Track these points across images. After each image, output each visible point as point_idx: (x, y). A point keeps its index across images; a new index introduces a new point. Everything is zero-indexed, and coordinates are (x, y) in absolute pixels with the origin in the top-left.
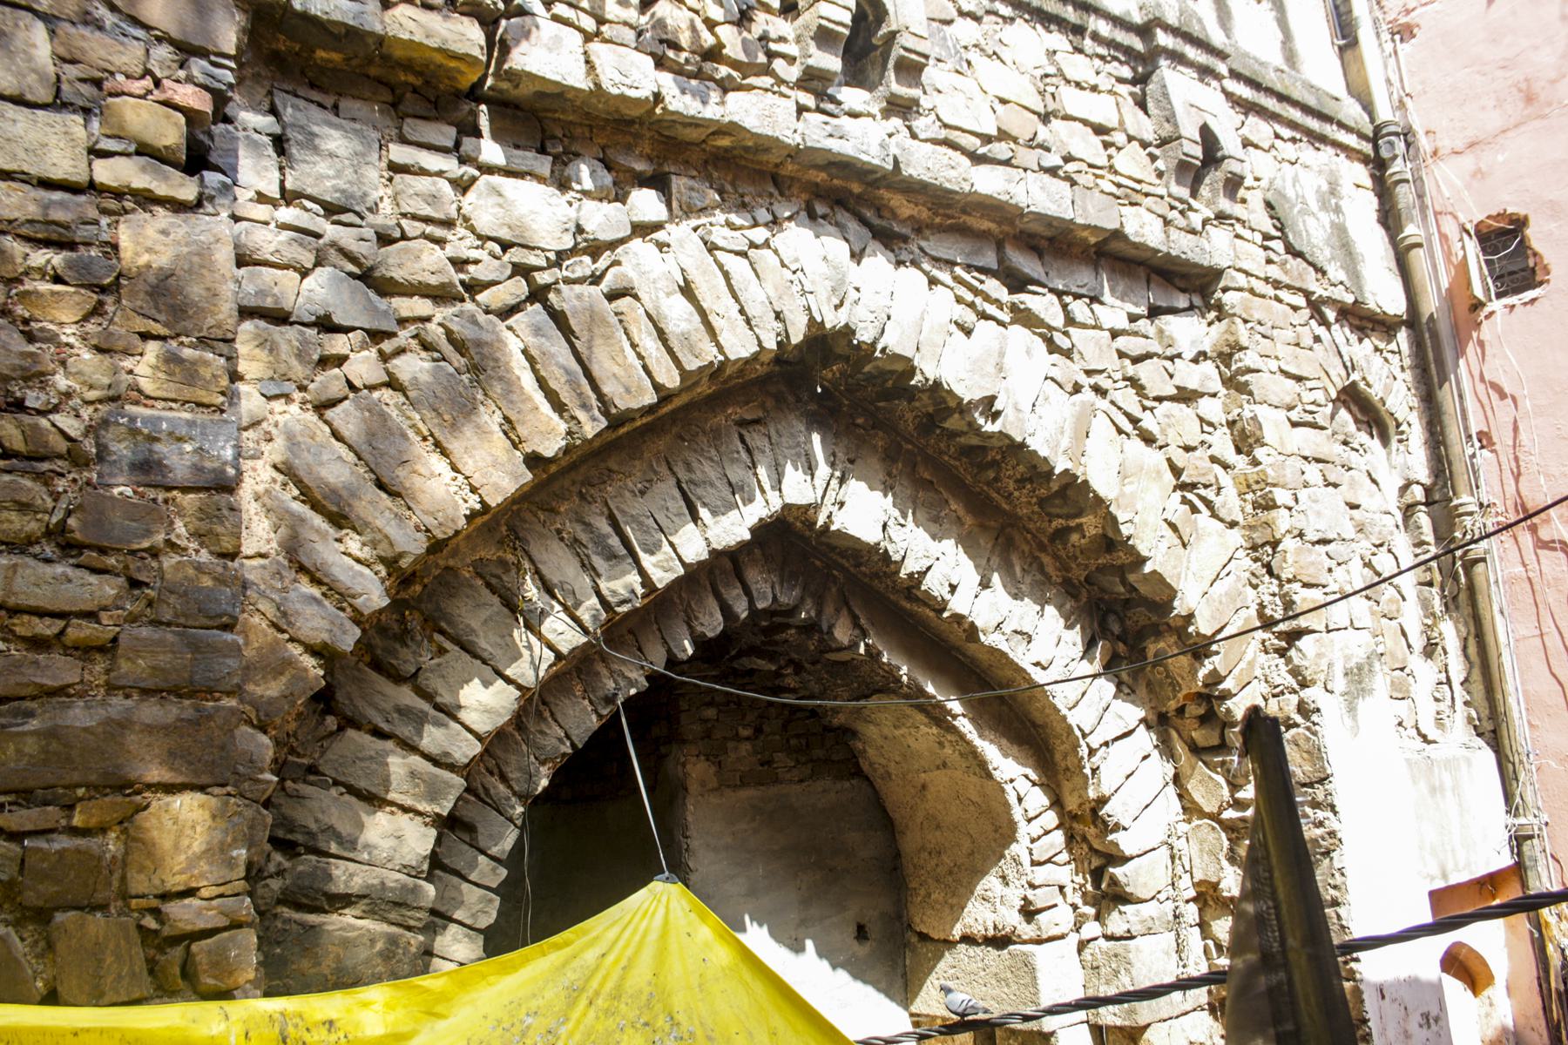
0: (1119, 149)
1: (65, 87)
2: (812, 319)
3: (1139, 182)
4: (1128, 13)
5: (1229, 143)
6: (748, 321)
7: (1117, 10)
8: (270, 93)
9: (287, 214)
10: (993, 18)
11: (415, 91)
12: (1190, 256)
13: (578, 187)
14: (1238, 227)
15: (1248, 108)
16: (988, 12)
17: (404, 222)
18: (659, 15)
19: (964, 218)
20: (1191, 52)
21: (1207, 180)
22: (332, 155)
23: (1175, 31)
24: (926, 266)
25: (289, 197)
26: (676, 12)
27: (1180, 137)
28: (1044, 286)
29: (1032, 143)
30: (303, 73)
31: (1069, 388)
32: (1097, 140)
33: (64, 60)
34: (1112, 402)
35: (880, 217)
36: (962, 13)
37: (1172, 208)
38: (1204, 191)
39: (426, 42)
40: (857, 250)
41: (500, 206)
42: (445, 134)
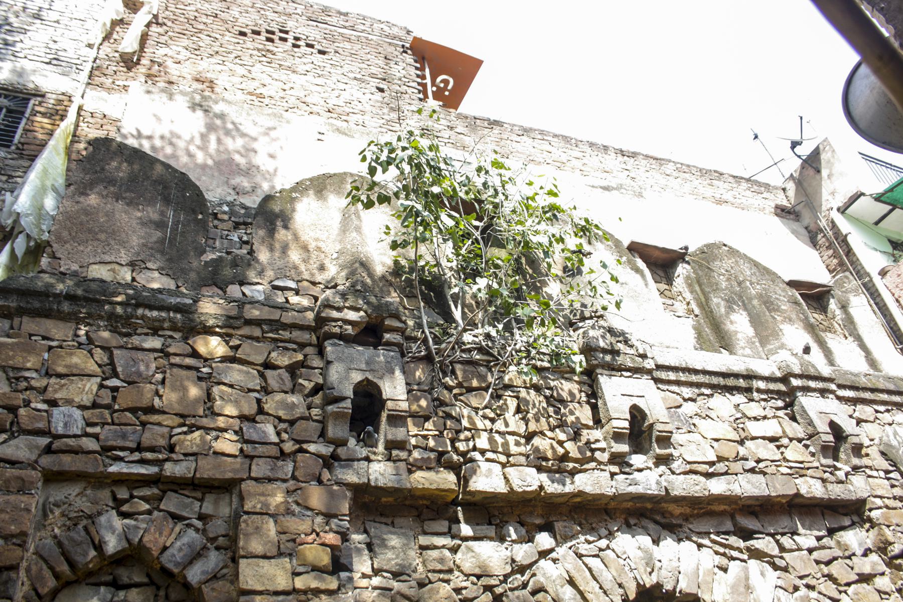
0: (786, 447)
1: (282, 546)
2: (638, 584)
3: (801, 462)
4: (773, 373)
5: (848, 426)
6: (605, 592)
7: (766, 373)
8: (364, 523)
9: (376, 581)
10: (702, 397)
11: (427, 507)
12: (843, 496)
13: (509, 539)
14: (868, 471)
15: (855, 401)
16: (699, 395)
17: (429, 575)
18: (535, 444)
19: (709, 507)
20: (812, 384)
21: (842, 450)
22: (393, 548)
23: (801, 376)
24: (694, 539)
25: (376, 572)
26: (543, 441)
27: (818, 433)
28: (762, 533)
29: (738, 458)
30: (377, 509)
31: (791, 590)
32: (772, 446)
33: (281, 533)
34: (820, 593)
35: (665, 517)
36: (685, 400)
37: (825, 472)
38: (842, 456)
39: (430, 487)
40: (656, 538)
41: (474, 557)
42: (443, 526)
